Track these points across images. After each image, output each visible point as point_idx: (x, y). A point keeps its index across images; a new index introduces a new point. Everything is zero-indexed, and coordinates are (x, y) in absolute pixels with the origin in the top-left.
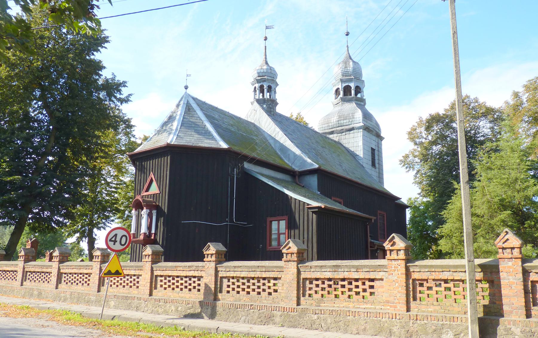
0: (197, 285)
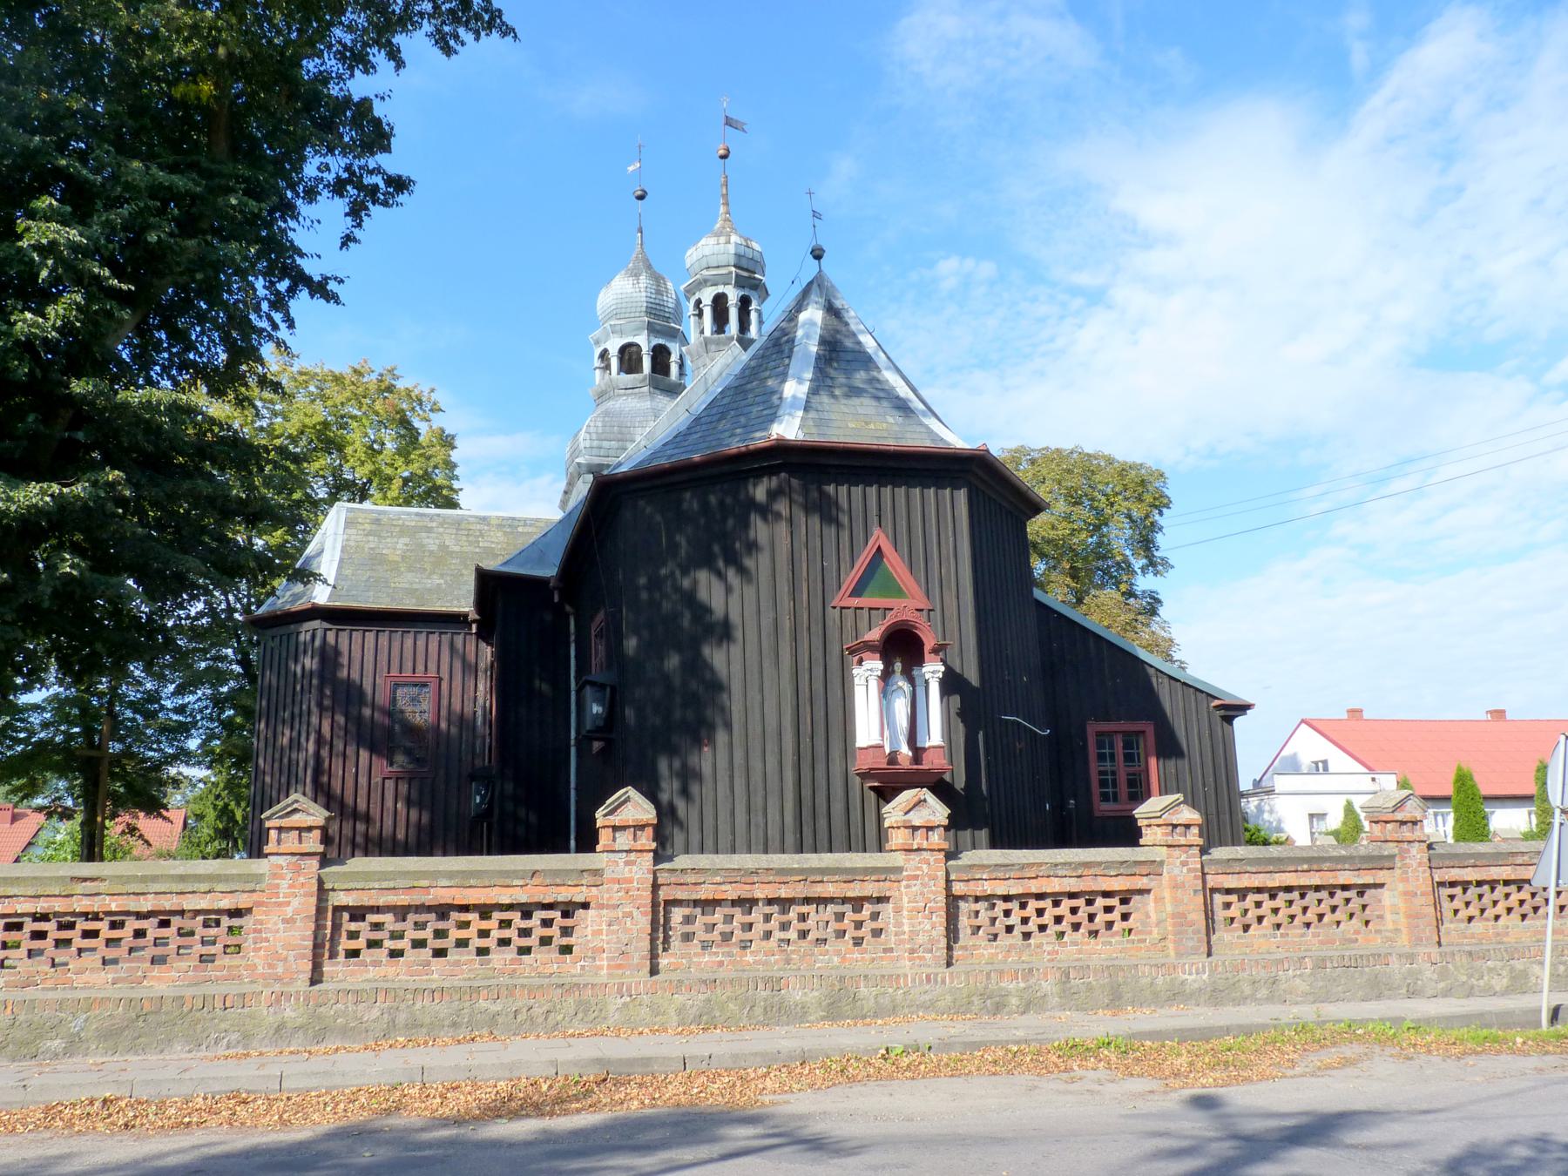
0: (492, 933)
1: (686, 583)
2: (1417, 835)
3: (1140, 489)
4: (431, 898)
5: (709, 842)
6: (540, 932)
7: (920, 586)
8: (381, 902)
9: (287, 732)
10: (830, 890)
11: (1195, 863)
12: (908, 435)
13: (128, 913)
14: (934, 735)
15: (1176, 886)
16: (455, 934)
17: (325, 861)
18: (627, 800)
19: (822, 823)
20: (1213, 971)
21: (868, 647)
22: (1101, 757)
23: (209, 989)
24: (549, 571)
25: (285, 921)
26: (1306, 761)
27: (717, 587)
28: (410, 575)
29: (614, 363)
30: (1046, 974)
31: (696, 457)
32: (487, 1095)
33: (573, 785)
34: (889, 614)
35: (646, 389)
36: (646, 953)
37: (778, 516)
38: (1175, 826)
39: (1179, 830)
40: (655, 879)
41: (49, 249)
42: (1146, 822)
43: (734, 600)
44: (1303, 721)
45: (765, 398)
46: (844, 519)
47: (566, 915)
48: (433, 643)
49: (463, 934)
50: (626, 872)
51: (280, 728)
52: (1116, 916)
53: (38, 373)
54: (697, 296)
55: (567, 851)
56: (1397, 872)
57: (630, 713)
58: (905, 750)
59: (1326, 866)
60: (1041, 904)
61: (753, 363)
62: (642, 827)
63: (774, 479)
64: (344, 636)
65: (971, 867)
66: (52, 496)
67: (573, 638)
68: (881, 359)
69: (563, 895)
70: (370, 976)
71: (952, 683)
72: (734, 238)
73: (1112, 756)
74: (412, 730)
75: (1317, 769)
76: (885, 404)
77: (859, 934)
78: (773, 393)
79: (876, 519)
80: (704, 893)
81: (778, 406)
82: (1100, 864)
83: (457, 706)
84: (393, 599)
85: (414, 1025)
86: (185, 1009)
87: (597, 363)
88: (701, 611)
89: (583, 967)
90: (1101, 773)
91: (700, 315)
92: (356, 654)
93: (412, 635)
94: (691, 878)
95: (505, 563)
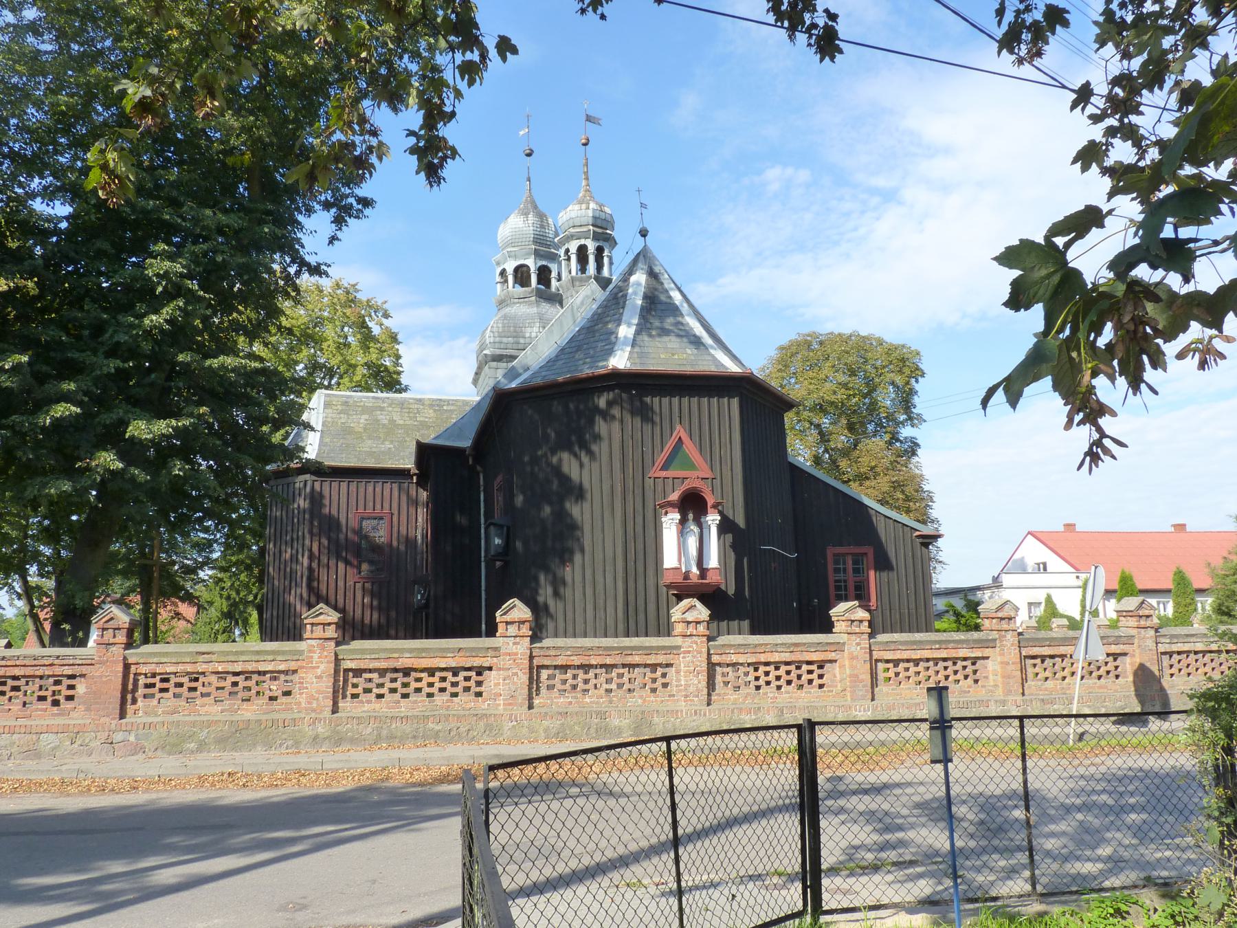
1: (555, 460)
2: (1012, 626)
3: (901, 364)
4: (399, 664)
5: (570, 629)
6: (463, 684)
7: (706, 462)
8: (371, 666)
9: (289, 550)
10: (636, 659)
11: (865, 643)
12: (700, 363)
13: (228, 673)
14: (713, 561)
15: (852, 658)
16: (414, 685)
17: (338, 644)
18: (515, 606)
19: (641, 617)
20: (875, 709)
21: (671, 504)
22: (837, 571)
23: (275, 716)
24: (466, 443)
25: (317, 677)
26: (1030, 563)
27: (575, 464)
28: (370, 442)
29: (511, 279)
30: (768, 711)
31: (560, 379)
32: (435, 773)
33: (483, 588)
34: (686, 482)
35: (534, 298)
36: (526, 696)
37: (613, 417)
38: (853, 621)
39: (855, 623)
40: (531, 653)
41: (166, 276)
42: (836, 618)
43: (586, 472)
44: (1029, 533)
45: (605, 337)
46: (657, 419)
47: (821, 667)
48: (389, 489)
49: (418, 685)
50: (514, 649)
51: (283, 548)
52: (814, 676)
53: (157, 349)
54: (566, 246)
55: (480, 636)
56: (998, 649)
57: (519, 545)
58: (695, 570)
59: (950, 646)
60: (767, 669)
61: (599, 311)
62: (523, 622)
63: (611, 393)
64: (326, 486)
65: (723, 646)
66: (172, 427)
67: (482, 488)
68: (685, 308)
69: (477, 662)
70: (366, 709)
71: (726, 526)
72: (592, 205)
73: (845, 570)
74: (376, 548)
75: (1039, 570)
76: (685, 340)
77: (655, 686)
78: (612, 333)
79: (678, 419)
80: (559, 662)
81: (615, 343)
82: (805, 644)
83: (403, 531)
84: (359, 459)
85: (391, 737)
86: (262, 727)
87: (498, 279)
88: (565, 480)
89: (489, 705)
90: (836, 581)
91: (569, 259)
92: (335, 497)
93: (372, 484)
94: (552, 653)
95: (435, 438)
